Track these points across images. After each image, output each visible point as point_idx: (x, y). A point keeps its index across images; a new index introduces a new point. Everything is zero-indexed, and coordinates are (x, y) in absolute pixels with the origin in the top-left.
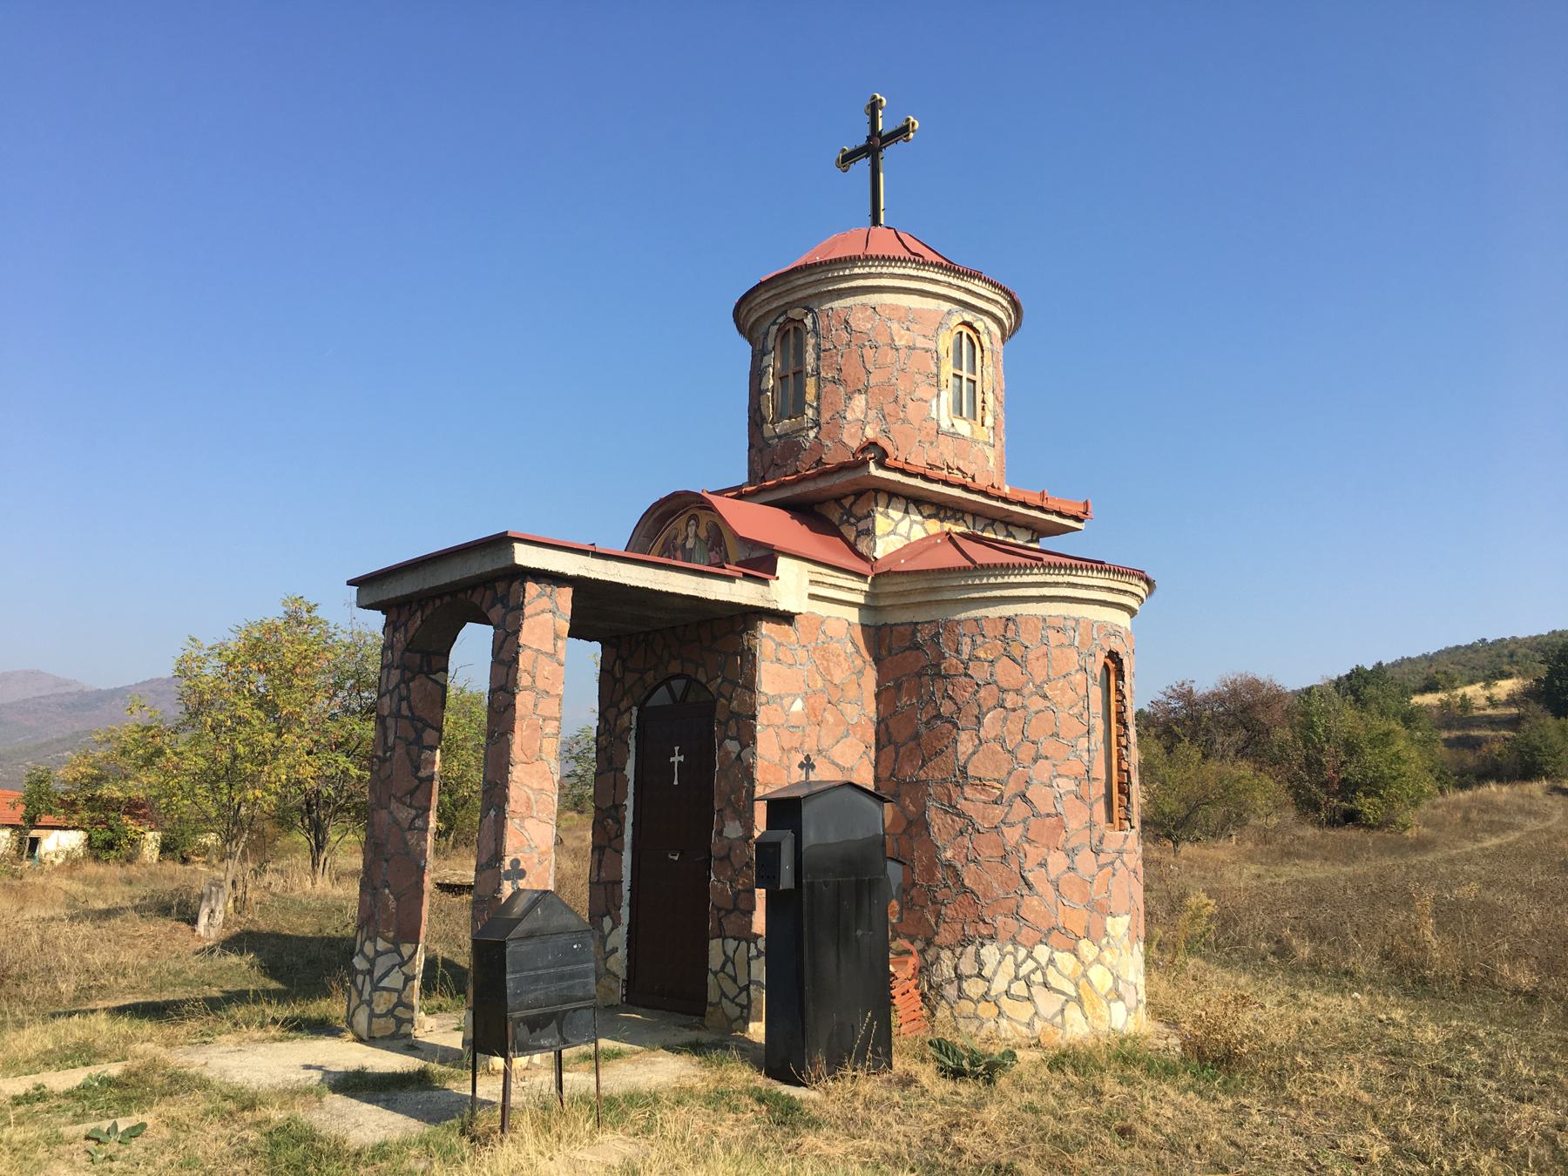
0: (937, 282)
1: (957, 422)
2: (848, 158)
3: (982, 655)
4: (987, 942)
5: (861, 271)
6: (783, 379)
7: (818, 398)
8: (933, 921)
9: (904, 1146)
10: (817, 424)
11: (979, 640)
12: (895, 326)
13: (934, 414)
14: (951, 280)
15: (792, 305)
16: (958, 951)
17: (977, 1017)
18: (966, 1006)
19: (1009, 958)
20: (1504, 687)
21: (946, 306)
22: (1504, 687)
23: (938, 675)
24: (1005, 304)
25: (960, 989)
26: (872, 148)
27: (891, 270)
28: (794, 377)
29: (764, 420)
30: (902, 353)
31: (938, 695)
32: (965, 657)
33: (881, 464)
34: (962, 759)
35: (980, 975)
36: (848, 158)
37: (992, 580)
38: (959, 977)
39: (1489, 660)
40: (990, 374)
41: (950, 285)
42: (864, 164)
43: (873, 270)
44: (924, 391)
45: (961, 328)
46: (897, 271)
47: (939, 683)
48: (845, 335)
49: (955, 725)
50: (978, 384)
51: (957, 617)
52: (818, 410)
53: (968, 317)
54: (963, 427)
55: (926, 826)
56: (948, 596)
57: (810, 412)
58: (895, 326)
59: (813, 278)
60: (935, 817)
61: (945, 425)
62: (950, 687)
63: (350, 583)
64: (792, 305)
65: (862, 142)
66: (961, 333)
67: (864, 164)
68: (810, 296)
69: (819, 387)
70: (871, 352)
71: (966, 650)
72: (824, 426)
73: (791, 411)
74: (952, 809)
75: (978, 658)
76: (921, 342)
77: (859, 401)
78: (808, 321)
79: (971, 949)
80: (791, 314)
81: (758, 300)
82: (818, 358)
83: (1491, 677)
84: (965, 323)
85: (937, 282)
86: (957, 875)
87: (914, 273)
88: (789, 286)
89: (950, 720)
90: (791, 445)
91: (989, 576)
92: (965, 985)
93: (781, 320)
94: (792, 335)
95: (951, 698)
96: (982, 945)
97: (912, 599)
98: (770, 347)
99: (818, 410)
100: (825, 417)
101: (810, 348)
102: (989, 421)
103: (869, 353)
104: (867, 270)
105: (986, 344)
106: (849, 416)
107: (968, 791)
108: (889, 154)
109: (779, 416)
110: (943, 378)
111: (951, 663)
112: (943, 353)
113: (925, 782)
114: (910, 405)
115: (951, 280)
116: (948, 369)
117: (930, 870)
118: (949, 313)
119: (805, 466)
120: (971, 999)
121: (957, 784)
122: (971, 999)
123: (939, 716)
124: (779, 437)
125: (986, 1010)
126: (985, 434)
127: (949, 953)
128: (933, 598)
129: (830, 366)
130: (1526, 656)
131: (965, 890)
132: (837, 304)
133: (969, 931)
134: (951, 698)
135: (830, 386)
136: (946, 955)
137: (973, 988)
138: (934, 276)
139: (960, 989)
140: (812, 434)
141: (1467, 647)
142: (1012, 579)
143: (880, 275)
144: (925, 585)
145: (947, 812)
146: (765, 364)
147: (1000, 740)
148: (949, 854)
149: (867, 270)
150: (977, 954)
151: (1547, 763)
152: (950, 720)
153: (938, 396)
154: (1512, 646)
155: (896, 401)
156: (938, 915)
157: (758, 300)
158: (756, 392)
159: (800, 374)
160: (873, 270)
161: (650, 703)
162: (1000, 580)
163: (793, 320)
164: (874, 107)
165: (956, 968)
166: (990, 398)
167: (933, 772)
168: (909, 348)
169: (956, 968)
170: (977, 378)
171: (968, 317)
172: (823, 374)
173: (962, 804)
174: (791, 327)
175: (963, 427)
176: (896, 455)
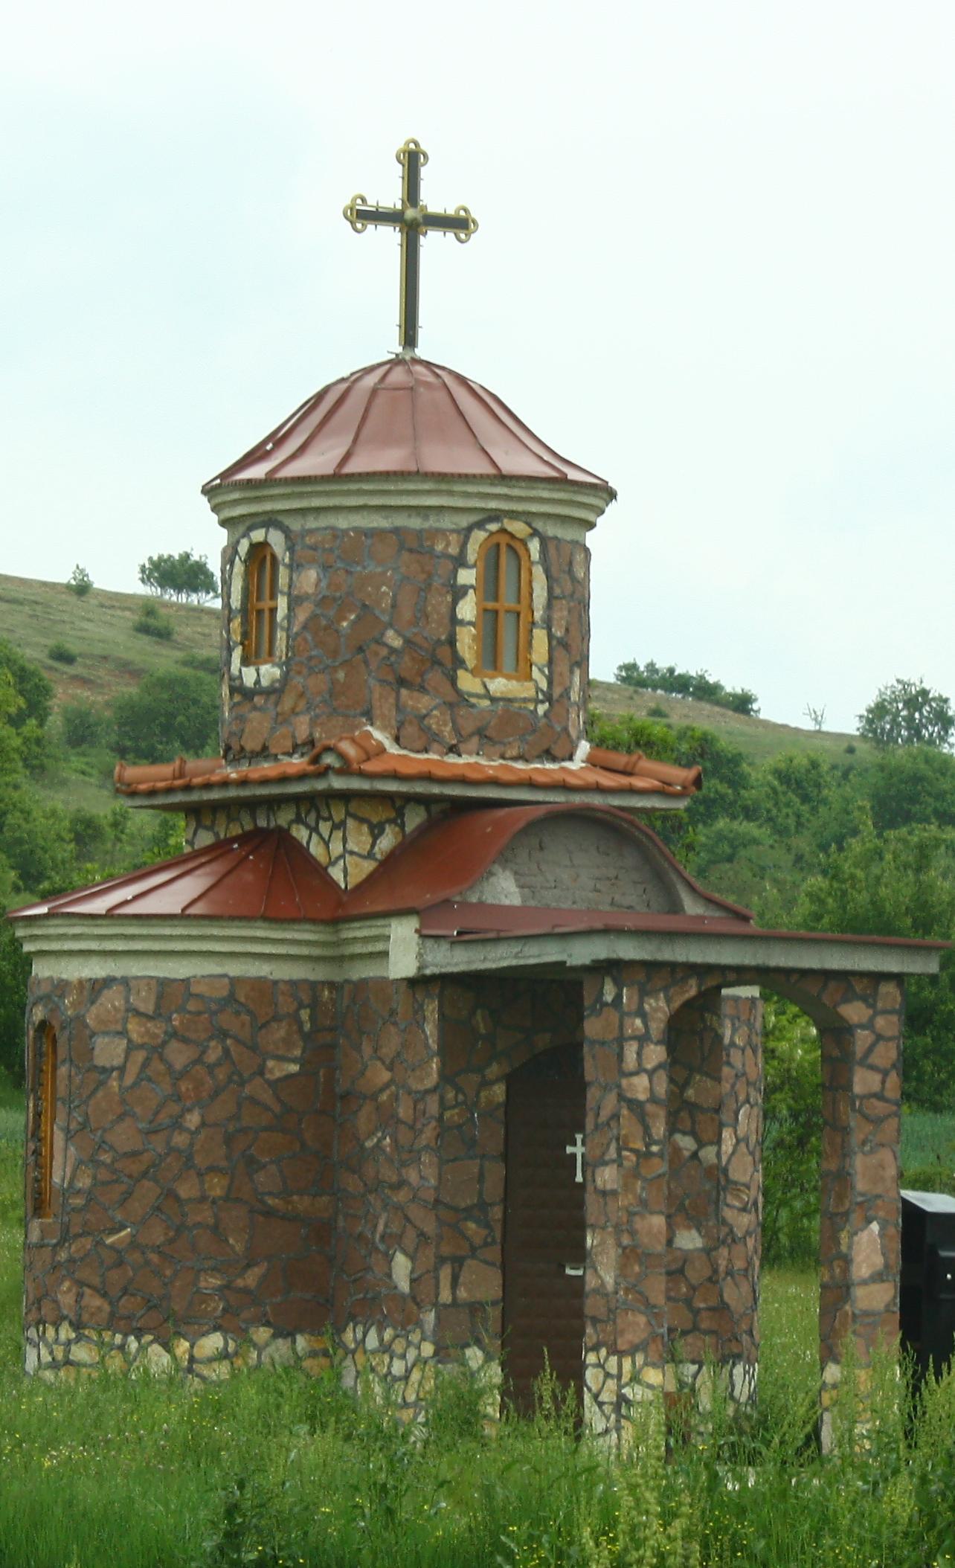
15: (513, 515)
64: (513, 515)
124: (494, 700)
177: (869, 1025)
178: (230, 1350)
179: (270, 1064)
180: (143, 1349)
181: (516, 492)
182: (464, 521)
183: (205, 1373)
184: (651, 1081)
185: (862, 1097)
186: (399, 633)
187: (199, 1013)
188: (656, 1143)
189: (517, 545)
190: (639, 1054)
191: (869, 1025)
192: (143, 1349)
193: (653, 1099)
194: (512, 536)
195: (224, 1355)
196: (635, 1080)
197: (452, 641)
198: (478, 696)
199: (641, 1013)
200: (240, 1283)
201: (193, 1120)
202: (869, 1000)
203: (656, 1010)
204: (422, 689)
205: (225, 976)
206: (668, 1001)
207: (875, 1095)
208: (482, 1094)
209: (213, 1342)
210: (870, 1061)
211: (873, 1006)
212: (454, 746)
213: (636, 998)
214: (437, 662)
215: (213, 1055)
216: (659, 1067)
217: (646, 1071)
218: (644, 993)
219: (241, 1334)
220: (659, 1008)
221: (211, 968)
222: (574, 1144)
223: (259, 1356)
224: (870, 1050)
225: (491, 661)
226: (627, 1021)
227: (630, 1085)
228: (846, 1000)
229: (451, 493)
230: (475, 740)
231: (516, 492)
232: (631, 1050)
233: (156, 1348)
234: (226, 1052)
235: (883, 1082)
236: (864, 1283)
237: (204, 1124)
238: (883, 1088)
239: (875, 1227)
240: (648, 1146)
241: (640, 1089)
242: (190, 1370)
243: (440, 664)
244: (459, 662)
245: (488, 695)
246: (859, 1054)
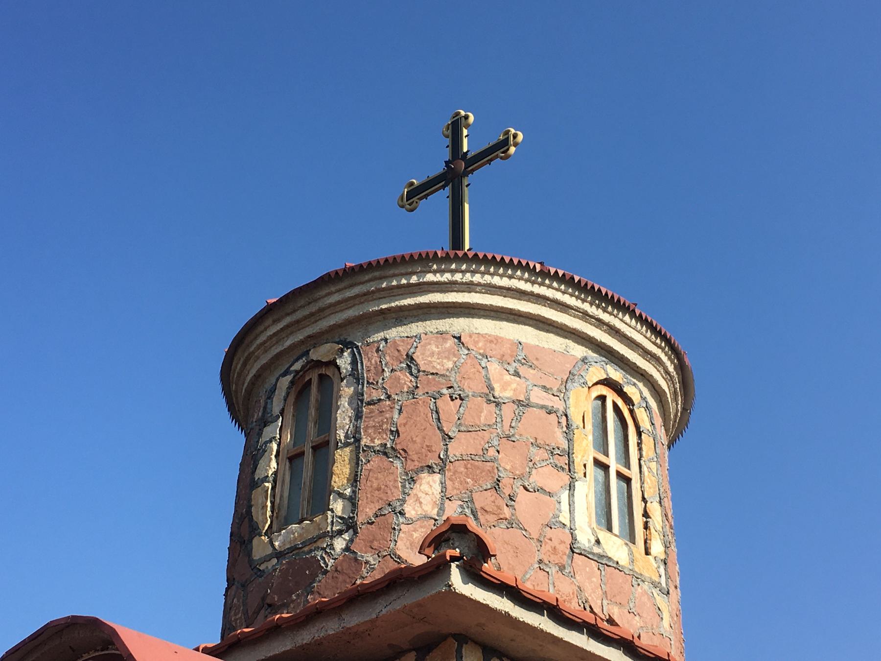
0: (564, 307)
1: (603, 535)
2: (417, 193)
5: (438, 278)
6: (294, 458)
7: (354, 480)
9: (407, 486)
10: (350, 524)
12: (494, 368)
13: (565, 518)
14: (586, 307)
15: (315, 340)
21: (579, 351)
24: (671, 368)
26: (453, 177)
27: (488, 279)
28: (313, 455)
29: (255, 530)
30: (508, 411)
33: (474, 575)
36: (417, 193)
40: (651, 474)
41: (585, 316)
42: (442, 198)
43: (458, 277)
44: (546, 476)
45: (603, 390)
46: (497, 281)
48: (407, 380)
50: (635, 485)
52: (353, 502)
53: (616, 374)
54: (615, 547)
57: (338, 506)
58: (494, 368)
59: (356, 290)
61: (585, 539)
64: (315, 340)
65: (439, 168)
66: (602, 398)
67: (442, 198)
69: (356, 462)
70: (453, 406)
72: (363, 530)
73: (304, 507)
76: (538, 397)
77: (429, 486)
78: (344, 362)
80: (316, 355)
81: (262, 338)
82: (358, 416)
84: (608, 382)
85: (564, 307)
87: (527, 287)
88: (313, 308)
90: (301, 564)
93: (297, 366)
94: (314, 386)
98: (276, 410)
99: (353, 502)
100: (366, 511)
101: (344, 403)
102: (657, 548)
103: (448, 407)
104: (447, 277)
105: (645, 424)
106: (410, 510)
108: (474, 185)
109: (281, 521)
110: (578, 460)
112: (576, 421)
114: (522, 495)
115: (586, 307)
116: (585, 450)
118: (584, 360)
119: (325, 591)
124: (279, 555)
126: (650, 567)
129: (379, 429)
132: (394, 333)
135: (376, 461)
138: (559, 296)
140: (339, 544)
143: (470, 287)
146: (265, 438)
149: (447, 277)
153: (571, 487)
155: (497, 485)
157: (262, 338)
158: (248, 482)
159: (324, 449)
160: (458, 277)
163: (319, 364)
164: (456, 126)
166: (655, 509)
168: (519, 403)
170: (633, 473)
171: (616, 374)
174: (314, 376)
175: (615, 547)
176: (503, 564)
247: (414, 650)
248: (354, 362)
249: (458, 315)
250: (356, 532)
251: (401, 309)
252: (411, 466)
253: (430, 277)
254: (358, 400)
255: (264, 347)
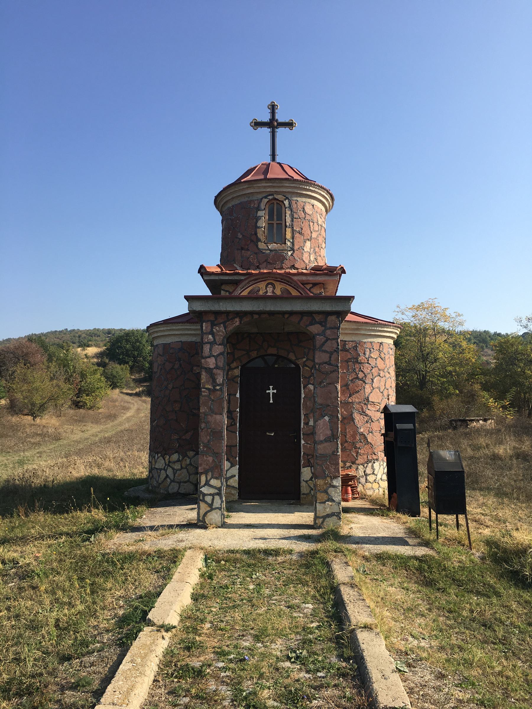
3: (373, 356)
4: (376, 461)
8: (355, 455)
10: (292, 249)
11: (372, 350)
15: (278, 193)
16: (365, 465)
17: (373, 488)
18: (369, 485)
19: (382, 466)
20: (92, 350)
22: (92, 350)
23: (357, 362)
25: (366, 479)
31: (357, 370)
32: (367, 356)
34: (367, 396)
35: (373, 473)
37: (380, 329)
38: (366, 475)
39: (83, 339)
47: (357, 366)
49: (364, 382)
51: (364, 341)
55: (353, 420)
56: (363, 332)
60: (357, 417)
62: (362, 367)
63: (187, 298)
64: (278, 193)
68: (288, 192)
71: (367, 353)
74: (363, 413)
75: (372, 357)
78: (286, 203)
79: (370, 464)
82: (292, 221)
83: (84, 345)
86: (365, 438)
89: (361, 380)
91: (379, 327)
92: (368, 478)
93: (270, 197)
95: (362, 371)
96: (374, 463)
97: (346, 332)
99: (293, 243)
100: (296, 247)
101: (288, 215)
107: (369, 406)
111: (362, 358)
113: (352, 403)
117: (354, 436)
120: (370, 483)
121: (365, 404)
122: (370, 483)
123: (357, 378)
124: (271, 250)
125: (375, 486)
127: (362, 466)
128: (356, 332)
130: (85, 338)
131: (368, 443)
133: (370, 458)
134: (362, 371)
136: (360, 467)
137: (371, 478)
139: (366, 479)
141: (60, 332)
142: (385, 329)
143: (317, 193)
144: (356, 327)
145: (361, 414)
147: (379, 388)
148: (362, 430)
150: (372, 466)
151: (118, 383)
152: (361, 380)
154: (80, 333)
156: (357, 453)
161: (249, 365)
162: (382, 329)
165: (365, 472)
167: (355, 399)
169: (365, 472)
172: (295, 228)
173: (368, 412)
177: (323, 333)
178: (181, 459)
179: (195, 368)
180: (158, 458)
181: (275, 185)
182: (260, 196)
183: (173, 466)
184: (216, 360)
185: (320, 364)
186: (241, 234)
187: (172, 353)
188: (218, 385)
189: (281, 203)
190: (211, 350)
191: (323, 333)
192: (158, 458)
193: (217, 367)
194: (277, 200)
195: (178, 461)
196: (208, 360)
197: (256, 234)
198: (265, 250)
199: (213, 334)
200: (184, 437)
201: (170, 386)
202: (322, 323)
203: (218, 331)
204: (248, 250)
205: (181, 341)
206: (225, 328)
207: (326, 363)
208: (230, 373)
209: (175, 457)
210: (323, 348)
211: (324, 326)
212: (258, 266)
213: (209, 328)
214: (252, 241)
215: (176, 366)
216: (222, 354)
217: (214, 356)
218: (213, 325)
219: (185, 455)
220: (220, 330)
221: (177, 339)
222: (273, 389)
223: (190, 461)
224: (323, 344)
225: (270, 239)
226: (205, 336)
227: (206, 362)
228: (311, 324)
229: (254, 188)
230: (265, 263)
231: (275, 185)
232: (206, 349)
233: (161, 458)
234: (181, 365)
235: (330, 357)
236: (321, 442)
237: (173, 388)
238: (330, 360)
239: (327, 418)
240: (214, 387)
241: (211, 364)
242: (169, 465)
243: (253, 241)
244: (259, 240)
245: (269, 249)
246: (318, 345)
247: (348, 539)
248: (289, 204)
249: (314, 199)
250: (294, 252)
251: (302, 193)
252: (305, 238)
253: (311, 188)
254: (293, 231)
255: (259, 187)
